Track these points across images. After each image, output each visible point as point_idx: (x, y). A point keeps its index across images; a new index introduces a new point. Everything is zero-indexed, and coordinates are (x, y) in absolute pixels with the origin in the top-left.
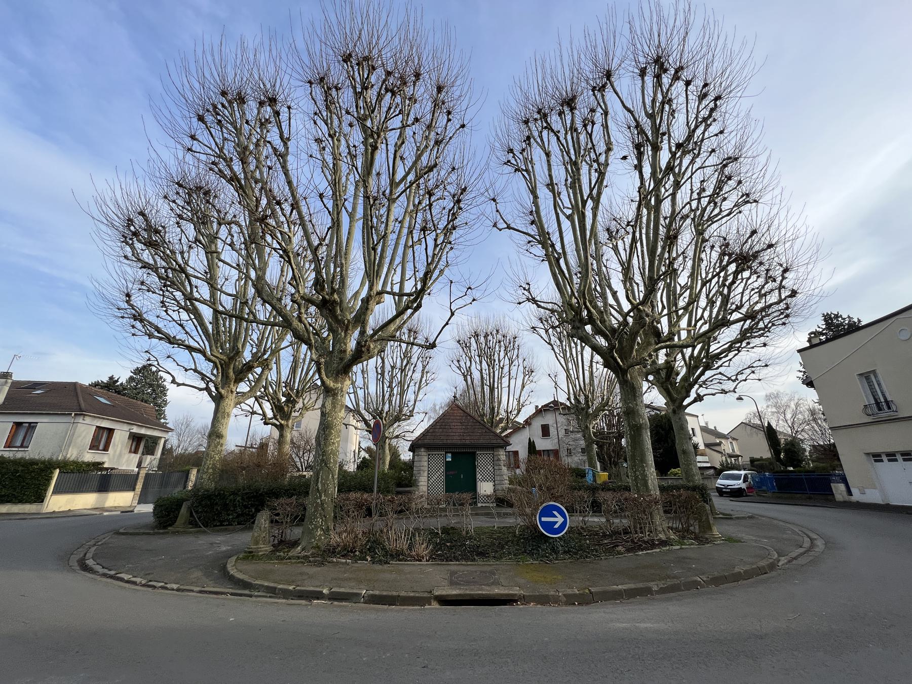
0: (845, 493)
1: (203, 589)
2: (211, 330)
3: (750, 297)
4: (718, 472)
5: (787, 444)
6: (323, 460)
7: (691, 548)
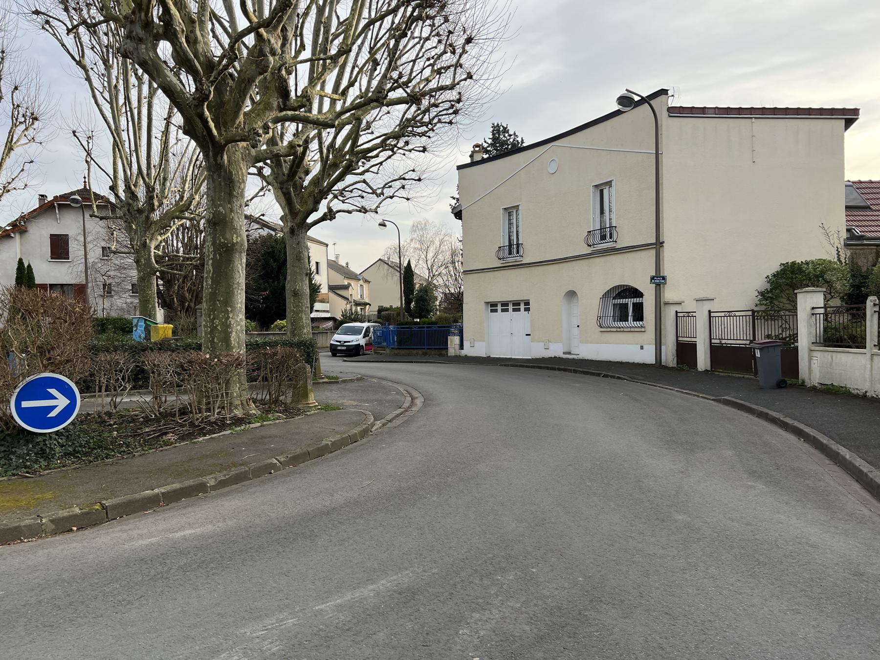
0: (457, 347)
3: (421, 72)
4: (337, 324)
5: (421, 290)
7: (277, 422)
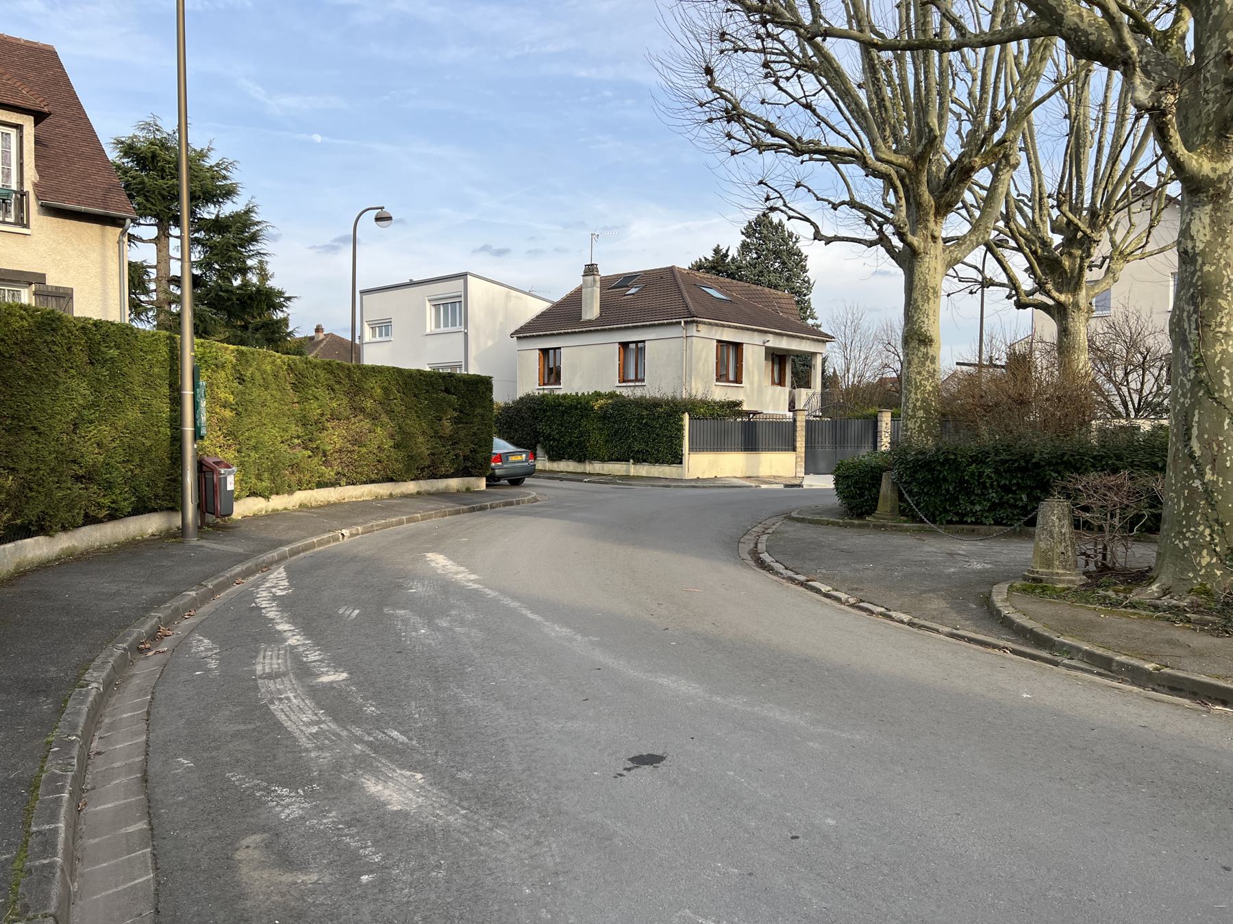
1: (955, 631)
2: (865, 102)
6: (1198, 382)
